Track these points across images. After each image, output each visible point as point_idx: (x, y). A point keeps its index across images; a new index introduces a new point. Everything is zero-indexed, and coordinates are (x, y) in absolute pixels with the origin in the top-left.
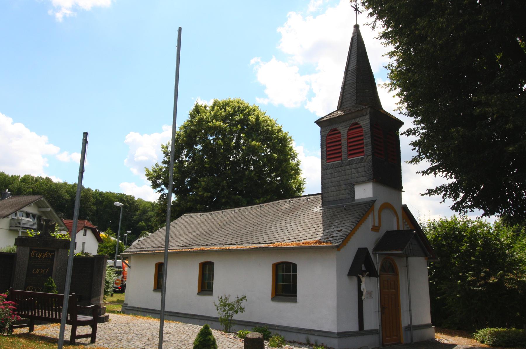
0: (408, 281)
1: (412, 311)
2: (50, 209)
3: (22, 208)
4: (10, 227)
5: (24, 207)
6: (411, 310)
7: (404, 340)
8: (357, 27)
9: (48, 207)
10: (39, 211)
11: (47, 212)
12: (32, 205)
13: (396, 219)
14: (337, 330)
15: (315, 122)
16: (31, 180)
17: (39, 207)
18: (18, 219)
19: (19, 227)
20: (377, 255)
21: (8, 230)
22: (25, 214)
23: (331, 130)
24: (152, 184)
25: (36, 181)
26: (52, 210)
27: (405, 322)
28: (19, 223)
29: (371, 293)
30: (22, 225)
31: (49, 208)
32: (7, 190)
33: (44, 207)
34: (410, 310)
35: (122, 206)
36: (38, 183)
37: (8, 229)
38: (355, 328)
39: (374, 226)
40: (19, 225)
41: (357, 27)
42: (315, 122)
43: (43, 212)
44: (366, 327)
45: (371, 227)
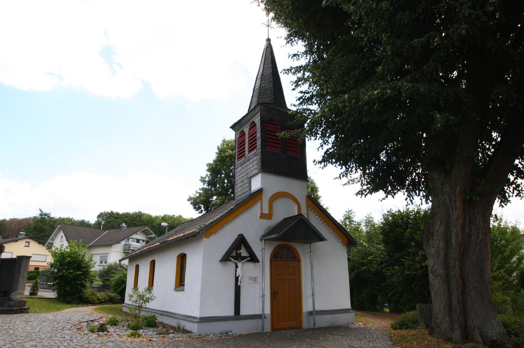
0: (312, 266)
1: (315, 296)
2: (153, 236)
3: (130, 236)
4: (124, 250)
5: (132, 235)
6: (314, 295)
7: (305, 325)
8: (269, 40)
9: (152, 234)
10: (147, 238)
11: (152, 237)
12: (139, 233)
13: (296, 207)
14: (200, 316)
15: (231, 127)
16: (168, 218)
17: (146, 235)
18: (129, 244)
19: (130, 250)
20: (263, 241)
21: (122, 253)
22: (135, 240)
23: (241, 132)
24: (193, 207)
25: (171, 218)
26: (155, 236)
27: (307, 306)
28: (130, 247)
29: (255, 278)
30: (132, 249)
31: (153, 234)
32: (124, 224)
33: (149, 235)
34: (313, 295)
35: (167, 225)
36: (172, 219)
37: (123, 251)
38: (231, 312)
39: (262, 214)
40: (129, 249)
41: (269, 40)
42: (231, 127)
43: (149, 238)
44: (244, 312)
45: (259, 215)
